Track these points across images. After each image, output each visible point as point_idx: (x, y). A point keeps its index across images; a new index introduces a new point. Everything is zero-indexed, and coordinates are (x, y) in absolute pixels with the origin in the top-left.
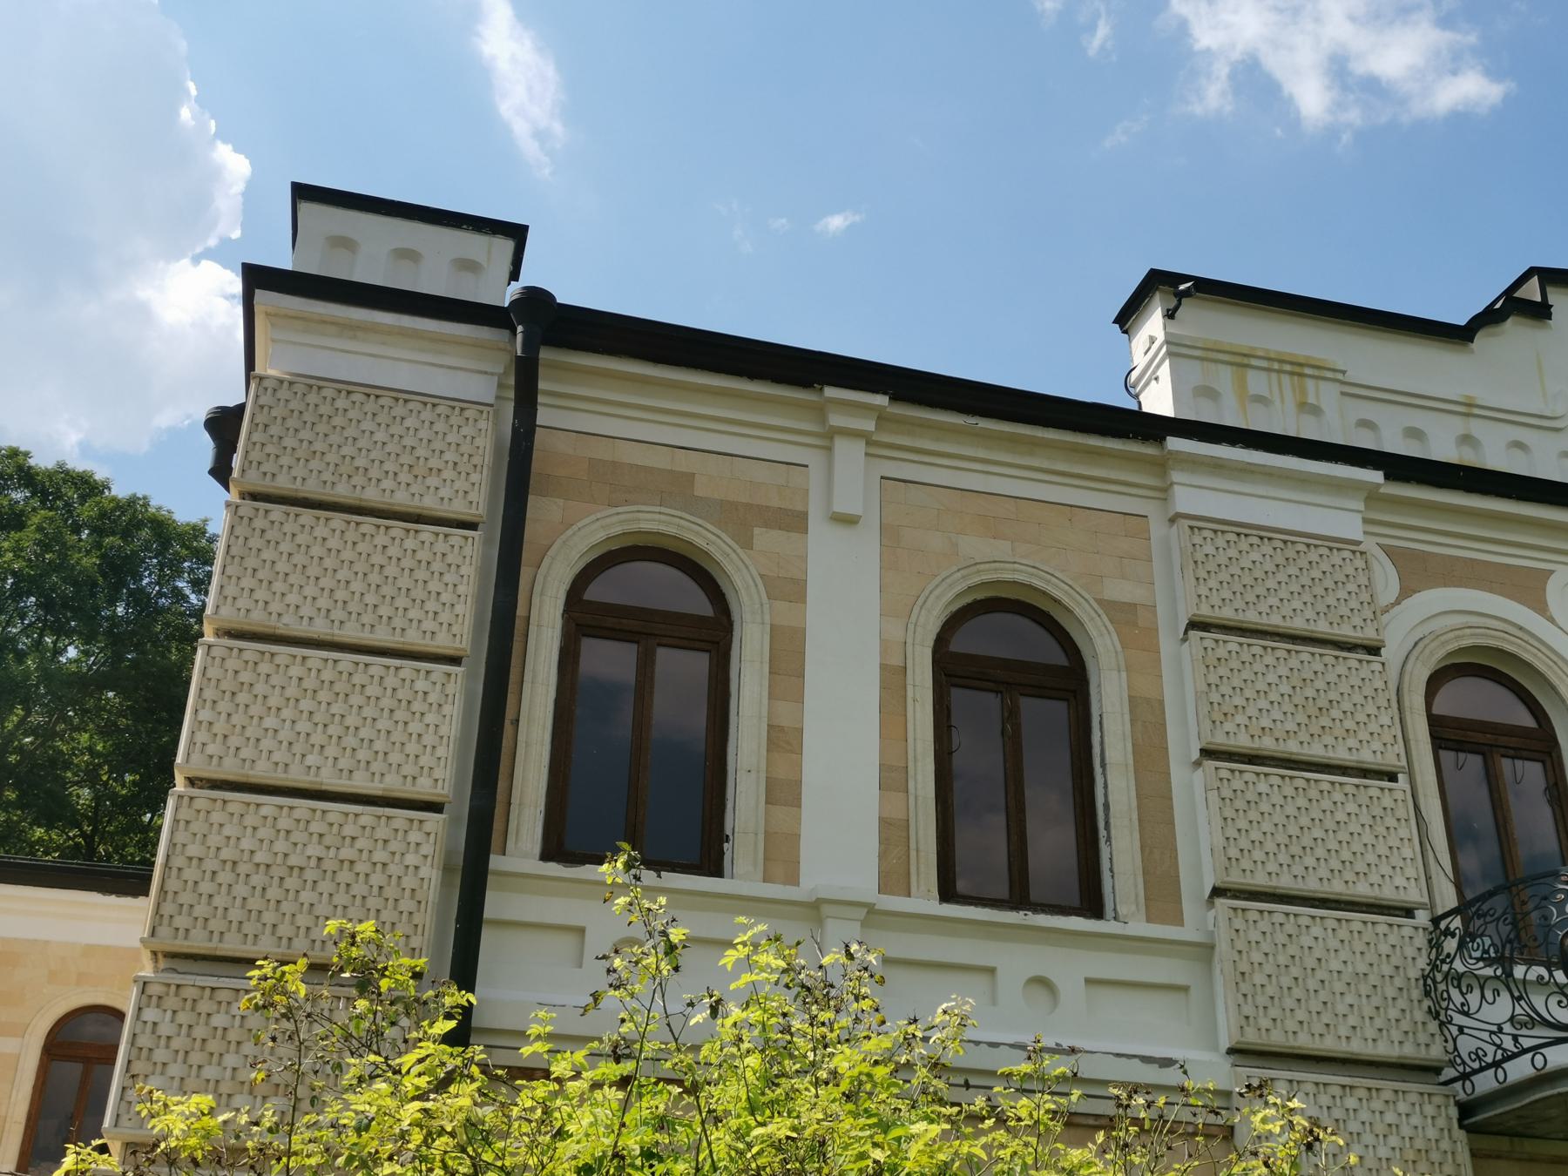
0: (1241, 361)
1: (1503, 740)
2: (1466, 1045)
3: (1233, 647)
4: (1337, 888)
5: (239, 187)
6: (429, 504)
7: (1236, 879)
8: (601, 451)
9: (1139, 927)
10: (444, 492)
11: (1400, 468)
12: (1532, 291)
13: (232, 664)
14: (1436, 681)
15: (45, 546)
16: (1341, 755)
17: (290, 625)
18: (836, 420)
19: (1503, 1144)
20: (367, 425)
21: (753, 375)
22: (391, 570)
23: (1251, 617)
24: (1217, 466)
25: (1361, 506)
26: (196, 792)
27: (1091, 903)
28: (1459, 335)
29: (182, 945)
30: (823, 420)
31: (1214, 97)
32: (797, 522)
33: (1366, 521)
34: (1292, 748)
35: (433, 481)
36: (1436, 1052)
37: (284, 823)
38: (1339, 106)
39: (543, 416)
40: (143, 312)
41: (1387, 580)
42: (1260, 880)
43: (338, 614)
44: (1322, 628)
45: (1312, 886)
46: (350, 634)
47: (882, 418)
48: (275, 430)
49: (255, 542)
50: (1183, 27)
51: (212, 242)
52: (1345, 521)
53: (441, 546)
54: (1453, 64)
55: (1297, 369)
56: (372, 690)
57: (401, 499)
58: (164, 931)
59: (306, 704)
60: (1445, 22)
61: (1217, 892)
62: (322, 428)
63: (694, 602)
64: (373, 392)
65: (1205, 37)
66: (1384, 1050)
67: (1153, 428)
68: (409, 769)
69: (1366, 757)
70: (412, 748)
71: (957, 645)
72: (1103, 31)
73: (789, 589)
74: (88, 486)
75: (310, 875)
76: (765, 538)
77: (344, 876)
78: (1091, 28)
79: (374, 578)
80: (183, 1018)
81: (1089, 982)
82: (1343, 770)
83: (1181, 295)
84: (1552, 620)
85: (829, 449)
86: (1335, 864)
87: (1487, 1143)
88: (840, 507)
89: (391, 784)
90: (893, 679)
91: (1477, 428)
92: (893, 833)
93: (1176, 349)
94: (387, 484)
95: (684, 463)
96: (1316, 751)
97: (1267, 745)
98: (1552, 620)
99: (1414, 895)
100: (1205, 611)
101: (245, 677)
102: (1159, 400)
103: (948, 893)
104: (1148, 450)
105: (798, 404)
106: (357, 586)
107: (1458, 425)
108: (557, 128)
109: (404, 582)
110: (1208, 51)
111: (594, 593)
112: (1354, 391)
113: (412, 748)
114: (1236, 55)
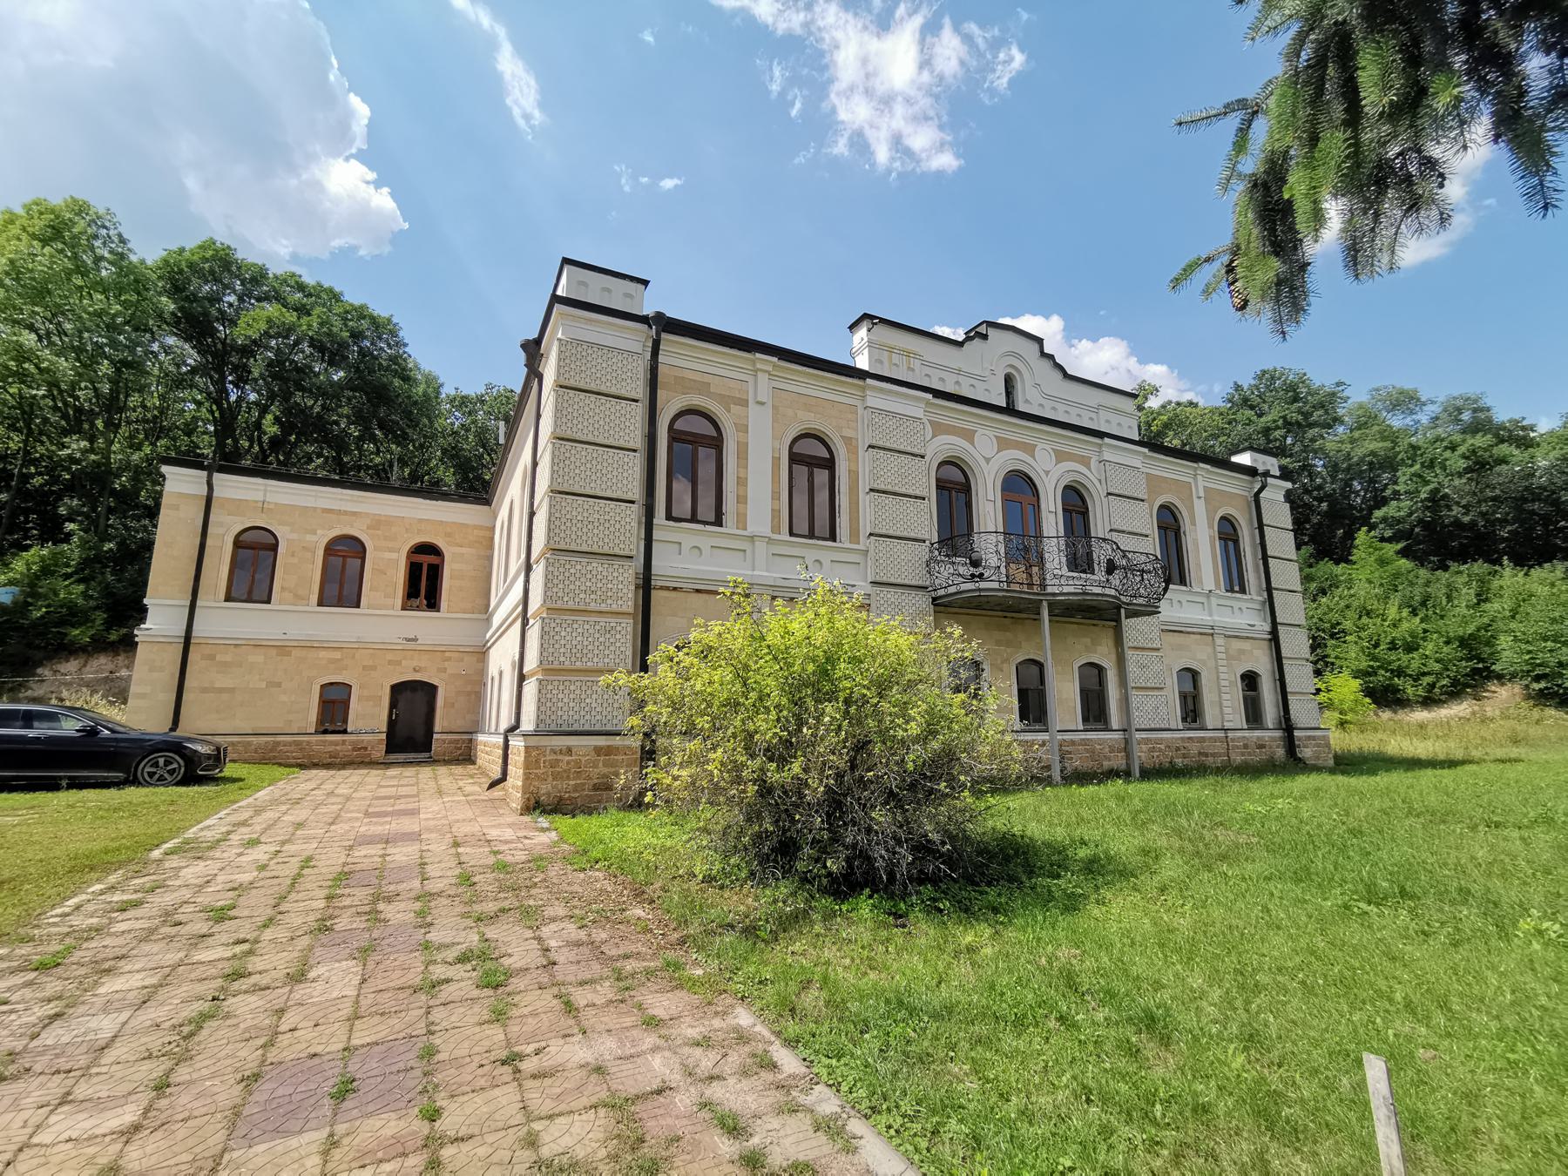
0: (891, 350)
2: (937, 582)
4: (905, 534)
5: (366, 121)
6: (623, 393)
7: (877, 531)
8: (679, 373)
9: (847, 545)
11: (938, 394)
12: (982, 329)
13: (562, 450)
14: (941, 464)
15: (322, 324)
16: (910, 492)
18: (759, 366)
19: (942, 609)
20: (600, 361)
22: (612, 417)
23: (888, 445)
24: (882, 390)
29: (557, 547)
30: (754, 365)
31: (841, 147)
32: (744, 403)
34: (897, 489)
35: (624, 384)
36: (928, 583)
37: (586, 507)
38: (893, 159)
39: (661, 359)
40: (318, 186)
42: (884, 532)
43: (596, 433)
44: (909, 449)
45: (898, 533)
46: (600, 440)
48: (567, 361)
49: (565, 405)
50: (834, 111)
51: (354, 151)
52: (919, 413)
53: (629, 409)
54: (941, 147)
55: (908, 354)
56: (610, 461)
57: (613, 391)
58: (552, 542)
59: (588, 465)
60: (941, 127)
61: (871, 534)
62: (584, 361)
63: (710, 431)
64: (600, 346)
65: (843, 115)
66: (914, 583)
67: (862, 374)
68: (625, 489)
69: (918, 493)
70: (625, 482)
72: (798, 105)
73: (744, 429)
74: (335, 297)
75: (596, 524)
77: (607, 525)
78: (793, 104)
79: (607, 420)
80: (561, 570)
82: (910, 496)
83: (874, 324)
87: (938, 608)
88: (759, 399)
90: (776, 461)
91: (961, 379)
92: (776, 513)
93: (871, 344)
94: (608, 384)
95: (707, 379)
96: (903, 491)
97: (889, 488)
99: (926, 536)
100: (874, 443)
101: (567, 455)
102: (862, 363)
103: (791, 534)
104: (860, 382)
105: (747, 359)
106: (601, 423)
107: (955, 378)
108: (537, 114)
109: (617, 422)
110: (843, 122)
113: (625, 482)
114: (855, 126)
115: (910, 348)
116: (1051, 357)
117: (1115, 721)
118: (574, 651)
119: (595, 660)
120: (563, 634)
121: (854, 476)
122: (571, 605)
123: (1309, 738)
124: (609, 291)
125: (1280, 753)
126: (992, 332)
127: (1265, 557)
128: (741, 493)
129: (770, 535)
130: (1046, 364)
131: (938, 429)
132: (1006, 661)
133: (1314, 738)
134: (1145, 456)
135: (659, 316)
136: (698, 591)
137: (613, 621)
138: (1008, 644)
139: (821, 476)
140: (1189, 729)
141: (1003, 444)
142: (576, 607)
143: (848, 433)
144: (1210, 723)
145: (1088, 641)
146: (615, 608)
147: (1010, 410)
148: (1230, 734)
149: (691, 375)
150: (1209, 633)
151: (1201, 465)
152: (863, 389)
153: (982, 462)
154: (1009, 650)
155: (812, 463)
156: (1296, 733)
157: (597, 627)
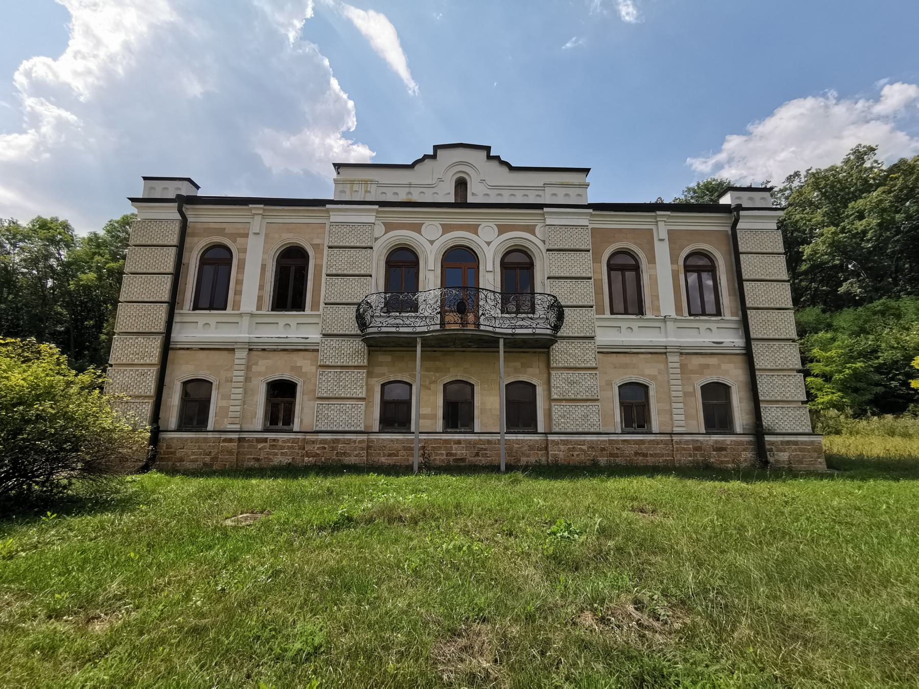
0: (352, 182)
1: (520, 266)
3: (583, 254)
8: (206, 226)
10: (344, 242)
11: (382, 204)
14: (507, 254)
17: (140, 271)
21: (235, 205)
23: (341, 244)
24: (340, 210)
25: (375, 214)
26: (326, 306)
27: (719, 313)
28: (412, 166)
30: (656, 219)
32: (246, 235)
33: (376, 217)
34: (345, 272)
41: (379, 230)
44: (358, 244)
45: (344, 301)
46: (151, 271)
47: (264, 210)
52: (372, 219)
55: (366, 182)
57: (160, 243)
63: (525, 259)
71: (688, 263)
73: (244, 250)
76: (239, 240)
81: (639, 327)
84: (422, 235)
85: (657, 225)
86: (583, 296)
88: (660, 238)
89: (157, 299)
91: (412, 190)
95: (224, 226)
97: (340, 272)
98: (422, 235)
103: (612, 313)
107: (407, 190)
111: (506, 261)
112: (379, 185)
115: (352, 178)
116: (497, 158)
117: (541, 429)
118: (123, 386)
119: (134, 391)
120: (118, 377)
121: (318, 268)
122: (124, 362)
123: (788, 443)
124: (527, 195)
125: (747, 456)
126: (439, 152)
127: (740, 281)
128: (238, 289)
129: (676, 317)
130: (494, 164)
131: (389, 227)
132: (434, 382)
133: (796, 443)
134: (591, 215)
135: (179, 196)
136: (202, 349)
137: (146, 369)
138: (437, 370)
139: (630, 275)
140: (628, 433)
141: (502, 229)
142: (128, 363)
143: (316, 241)
144: (655, 427)
145: (518, 364)
146: (148, 361)
147: (461, 203)
148: (675, 438)
149: (212, 226)
150: (660, 352)
151: (658, 213)
152: (543, 215)
153: (484, 246)
154: (437, 374)
155: (623, 269)
156: (767, 438)
157: (137, 373)
